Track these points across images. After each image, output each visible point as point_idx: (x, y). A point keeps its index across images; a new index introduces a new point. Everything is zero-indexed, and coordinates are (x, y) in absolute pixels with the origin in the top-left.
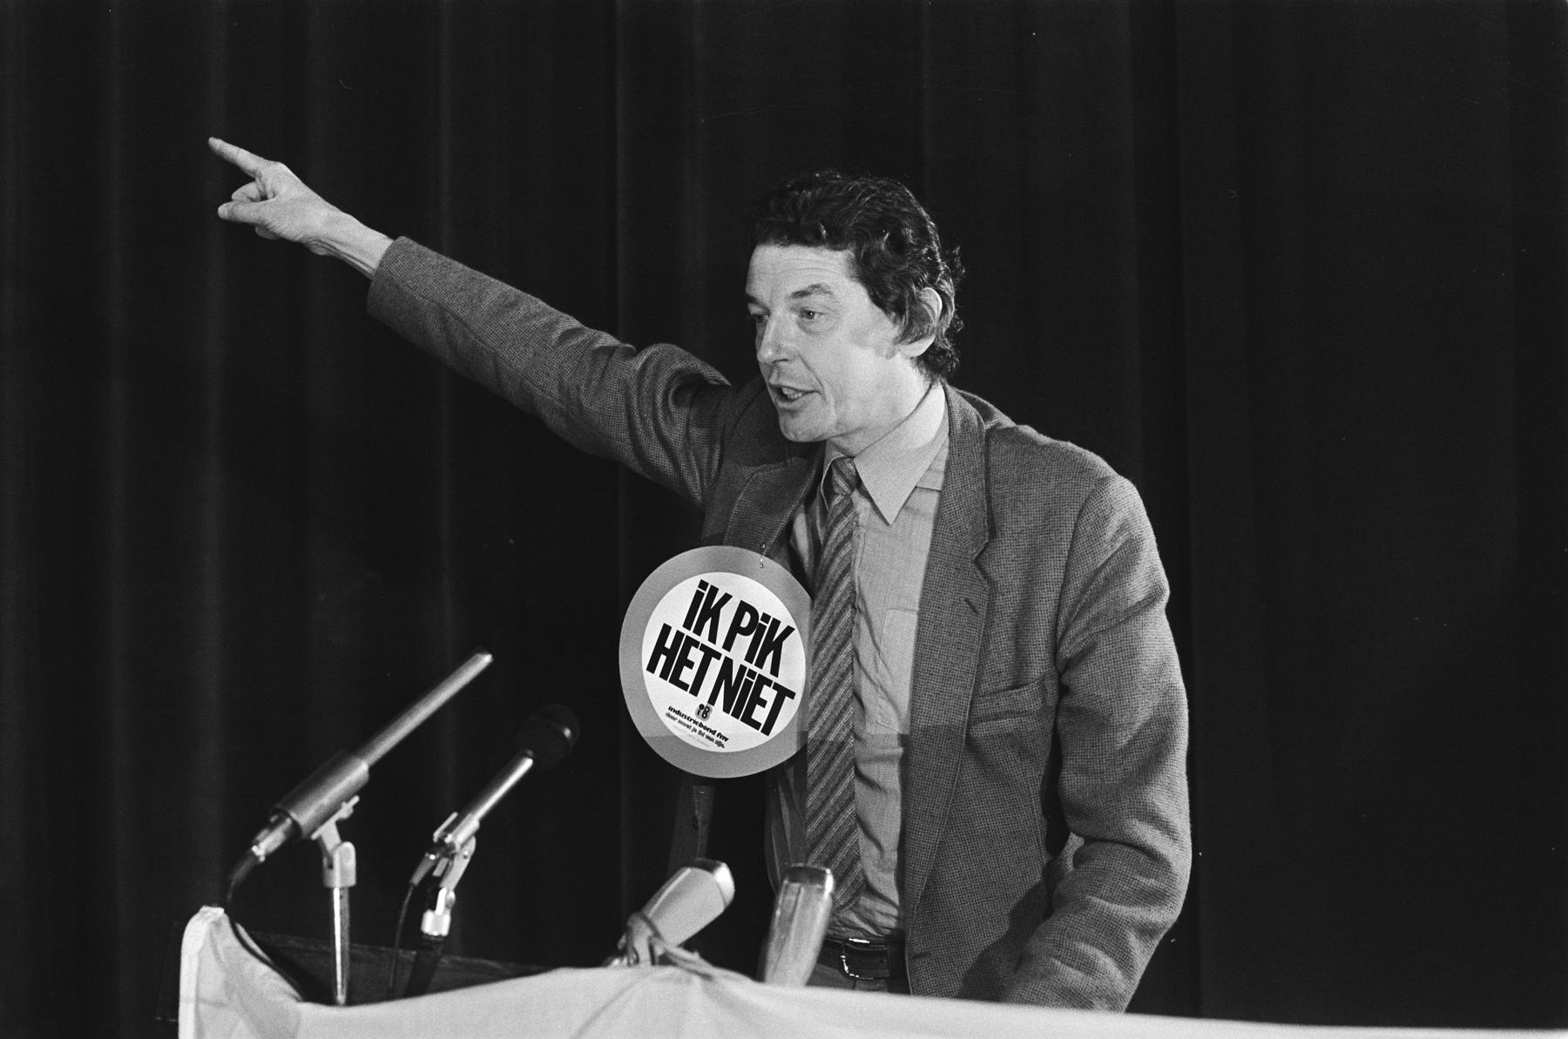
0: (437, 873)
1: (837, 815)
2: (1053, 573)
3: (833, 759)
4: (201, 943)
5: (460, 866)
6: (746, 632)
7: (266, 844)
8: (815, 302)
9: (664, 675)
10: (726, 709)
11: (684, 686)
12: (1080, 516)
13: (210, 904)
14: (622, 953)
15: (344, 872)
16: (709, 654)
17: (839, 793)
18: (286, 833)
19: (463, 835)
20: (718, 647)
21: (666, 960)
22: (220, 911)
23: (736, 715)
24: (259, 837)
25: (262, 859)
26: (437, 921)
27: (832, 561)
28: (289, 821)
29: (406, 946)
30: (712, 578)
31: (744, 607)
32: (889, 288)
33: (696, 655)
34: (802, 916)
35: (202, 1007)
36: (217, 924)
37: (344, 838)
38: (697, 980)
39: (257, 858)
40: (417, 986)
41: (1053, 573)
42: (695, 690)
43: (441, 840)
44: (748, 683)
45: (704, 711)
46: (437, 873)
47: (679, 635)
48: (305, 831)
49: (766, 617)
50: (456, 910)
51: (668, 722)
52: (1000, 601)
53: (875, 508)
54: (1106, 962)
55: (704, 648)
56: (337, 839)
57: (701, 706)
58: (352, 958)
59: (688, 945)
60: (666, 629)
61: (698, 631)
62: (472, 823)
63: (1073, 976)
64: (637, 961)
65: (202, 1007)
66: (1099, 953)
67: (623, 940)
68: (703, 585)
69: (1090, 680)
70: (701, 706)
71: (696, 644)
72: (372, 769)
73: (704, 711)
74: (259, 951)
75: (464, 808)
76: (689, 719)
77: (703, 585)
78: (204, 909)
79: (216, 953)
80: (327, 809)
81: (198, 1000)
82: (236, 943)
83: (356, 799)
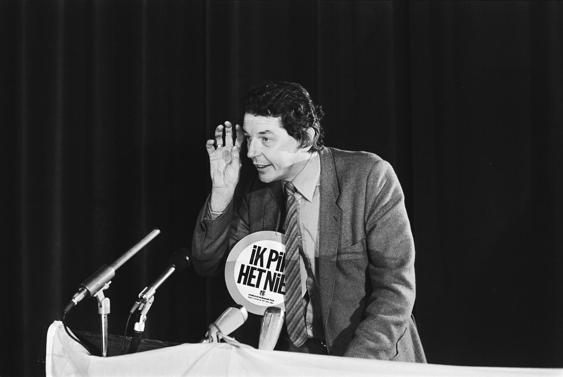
0: (140, 309)
1: (297, 311)
2: (362, 202)
3: (294, 291)
4: (54, 334)
5: (148, 306)
6: (274, 260)
7: (78, 298)
8: (267, 135)
9: (244, 283)
10: (271, 290)
11: (253, 285)
12: (368, 180)
13: (57, 320)
14: (207, 338)
15: (106, 308)
16: (261, 271)
17: (297, 303)
18: (85, 294)
19: (149, 295)
20: (264, 268)
21: (223, 341)
22: (61, 323)
23: (275, 291)
24: (75, 296)
25: (76, 304)
26: (140, 327)
27: (290, 220)
28: (86, 290)
29: (129, 335)
30: (258, 244)
31: (272, 251)
32: (294, 129)
33: (256, 273)
34: (273, 325)
35: (54, 357)
36: (60, 327)
37: (106, 296)
38: (234, 347)
39: (74, 303)
40: (133, 350)
41: (362, 202)
42: (258, 286)
43: (142, 297)
44: (278, 279)
45: (263, 293)
46: (140, 309)
47: (248, 267)
48: (92, 294)
49: (281, 253)
50: (147, 323)
51: (249, 300)
52: (344, 215)
53: (303, 197)
54: (384, 338)
55: (259, 270)
56: (104, 297)
57: (261, 291)
58: (109, 340)
59: (231, 335)
60: (243, 266)
61: (256, 264)
62: (153, 291)
63: (372, 344)
64: (213, 341)
65: (54, 357)
66: (381, 334)
67: (207, 333)
68: (255, 247)
69: (377, 240)
70: (261, 291)
71: (255, 269)
72: (116, 271)
73: (263, 293)
74: (75, 337)
75: (150, 285)
76: (257, 297)
77: (255, 247)
78: (55, 321)
79: (59, 337)
80: (100, 285)
81: (53, 354)
82: (67, 334)
83: (110, 282)
